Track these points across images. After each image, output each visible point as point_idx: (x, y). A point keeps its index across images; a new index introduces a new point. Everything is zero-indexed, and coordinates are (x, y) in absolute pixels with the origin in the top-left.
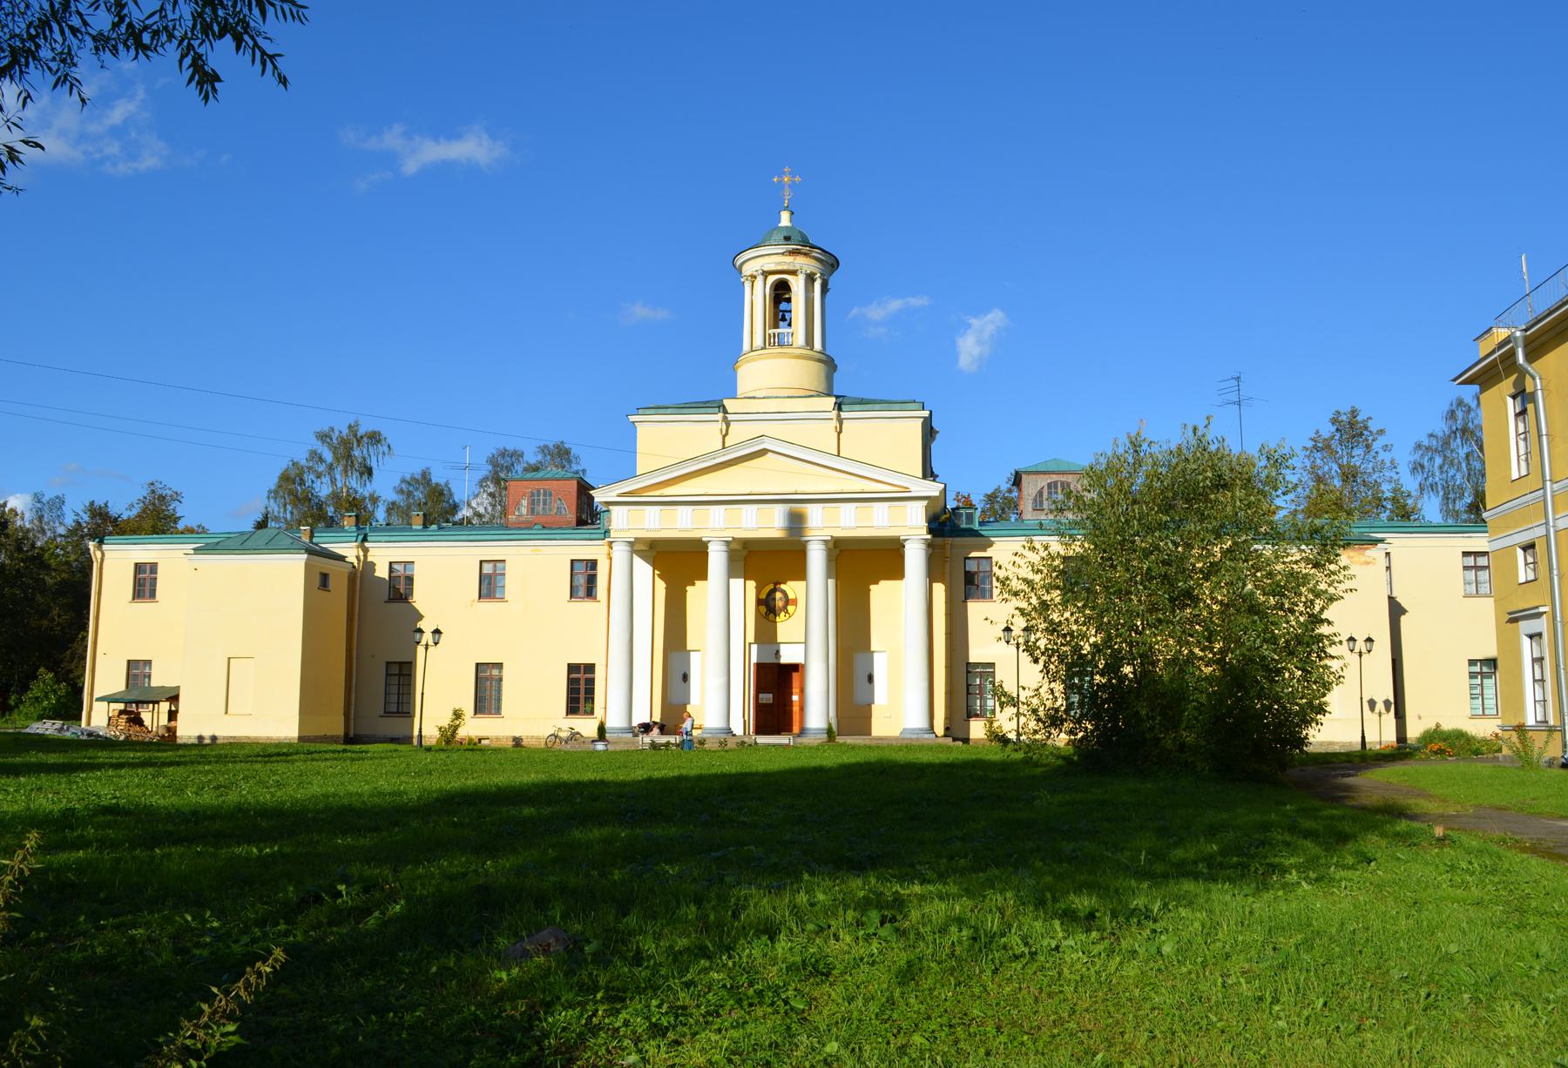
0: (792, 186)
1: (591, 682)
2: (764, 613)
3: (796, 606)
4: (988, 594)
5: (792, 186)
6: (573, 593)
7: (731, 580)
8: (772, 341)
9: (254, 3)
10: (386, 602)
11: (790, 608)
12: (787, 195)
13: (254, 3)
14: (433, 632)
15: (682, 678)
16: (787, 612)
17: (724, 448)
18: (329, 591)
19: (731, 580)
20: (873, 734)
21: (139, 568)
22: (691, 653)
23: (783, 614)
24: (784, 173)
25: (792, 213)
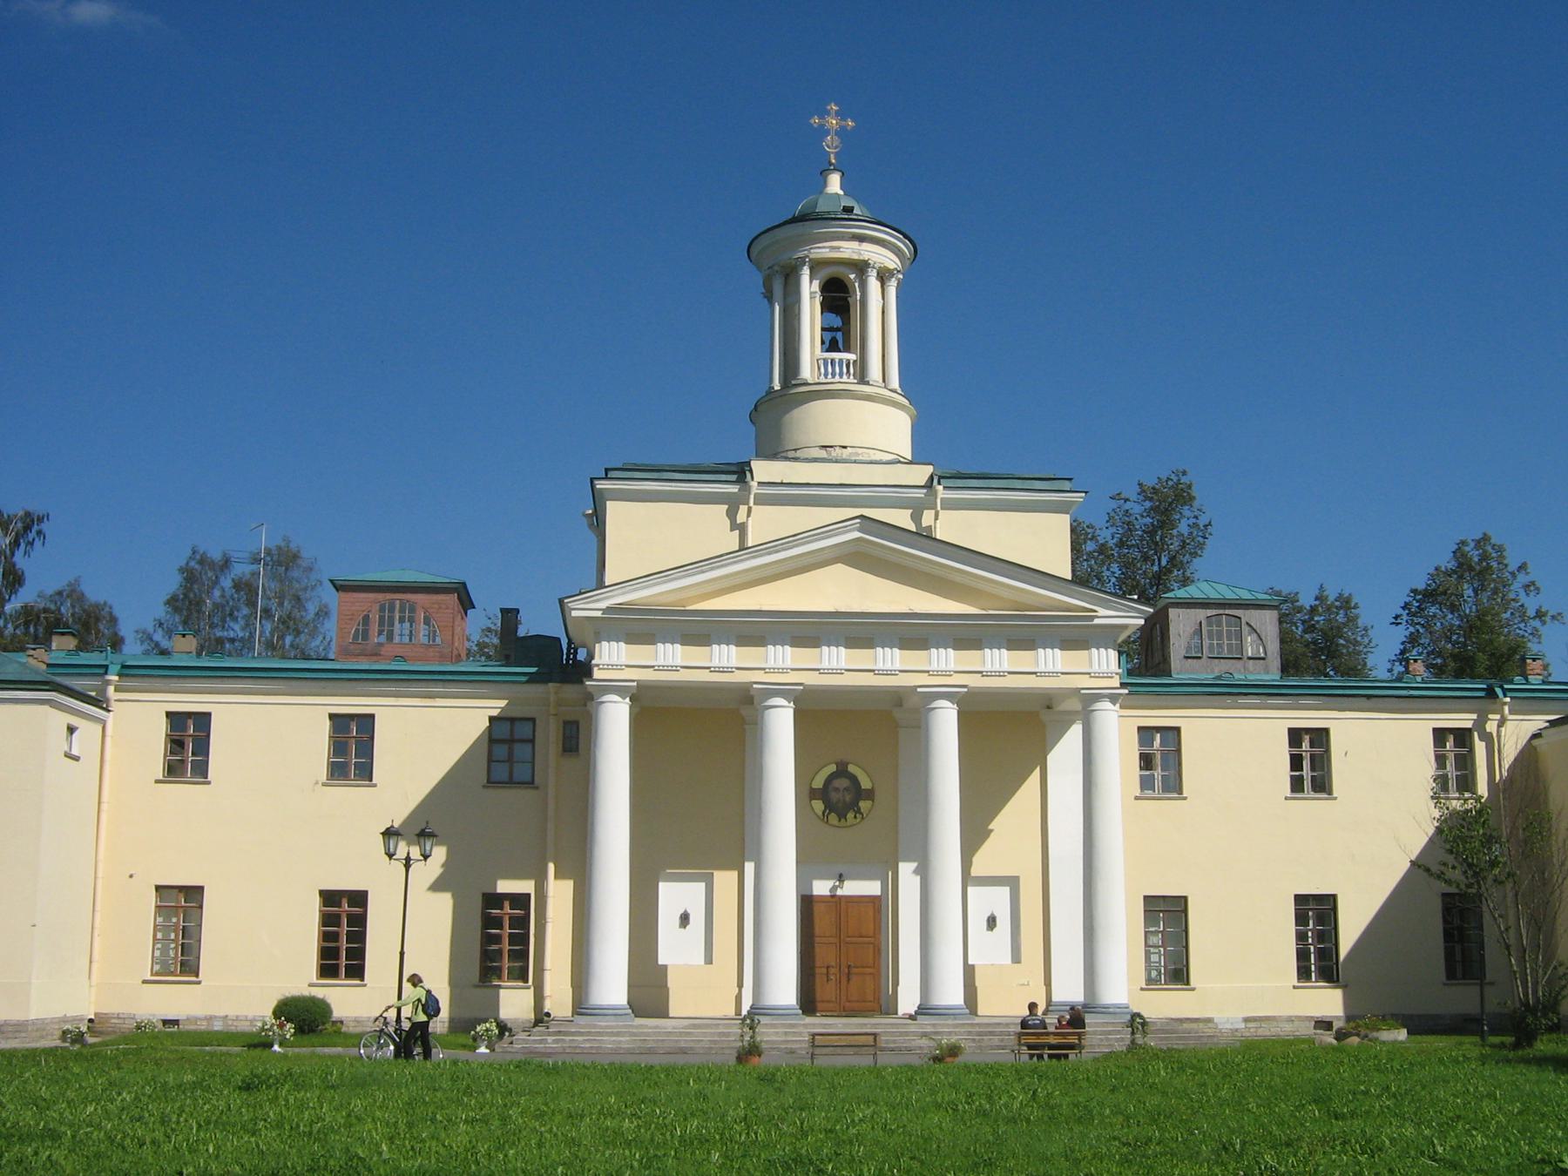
0: (841, 132)
1: (359, 921)
2: (820, 813)
3: (873, 801)
4: (501, 772)
5: (841, 132)
6: (1297, 785)
7: (671, 1015)
8: (822, 370)
9: (1096, 1175)
10: (157, 781)
11: (864, 805)
12: (831, 145)
13: (1096, 1175)
14: (382, 834)
15: (677, 921)
16: (859, 811)
17: (742, 547)
18: (1335, 798)
19: (671, 1015)
20: (879, 894)
21: (339, 722)
22: (700, 887)
23: (850, 815)
24: (828, 113)
25: (843, 174)
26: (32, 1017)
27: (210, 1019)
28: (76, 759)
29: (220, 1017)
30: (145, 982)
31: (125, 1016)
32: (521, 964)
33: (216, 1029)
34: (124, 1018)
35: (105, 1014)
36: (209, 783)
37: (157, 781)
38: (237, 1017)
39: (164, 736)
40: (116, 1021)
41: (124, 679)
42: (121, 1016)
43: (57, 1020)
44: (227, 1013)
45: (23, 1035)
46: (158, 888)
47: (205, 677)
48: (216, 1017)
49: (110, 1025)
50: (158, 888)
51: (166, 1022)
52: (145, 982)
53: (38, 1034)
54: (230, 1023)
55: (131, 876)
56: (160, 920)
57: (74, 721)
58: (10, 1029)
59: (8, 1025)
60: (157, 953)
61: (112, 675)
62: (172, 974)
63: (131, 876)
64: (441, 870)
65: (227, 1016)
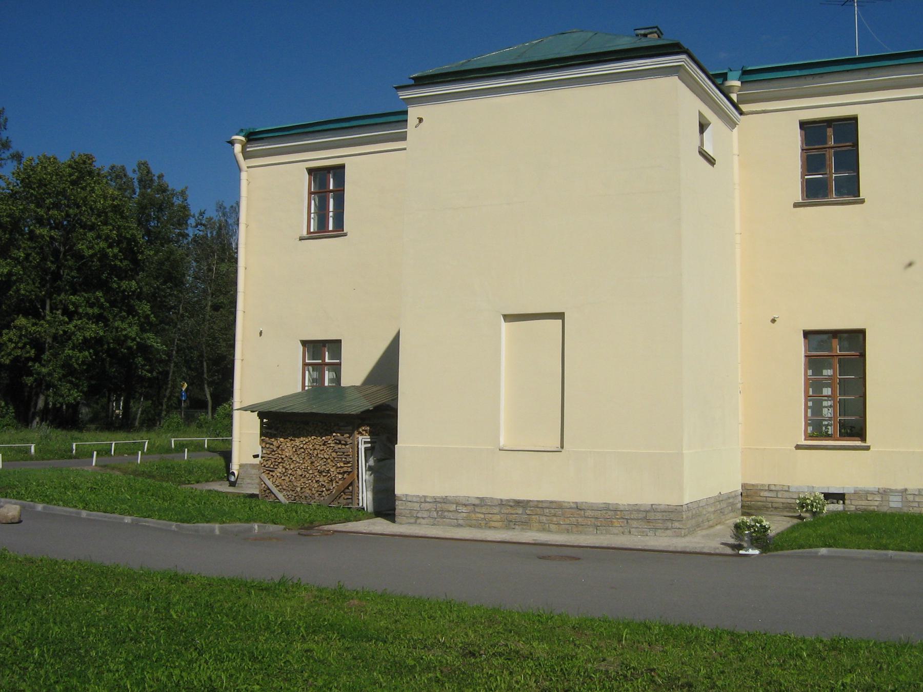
10: (796, 205)
26: (686, 500)
27: (885, 493)
28: (711, 161)
29: (896, 491)
30: (798, 447)
31: (778, 488)
32: (206, 386)
33: (892, 505)
34: (777, 491)
35: (753, 485)
36: (862, 201)
37: (796, 205)
38: (482, 499)
39: (800, 151)
40: (766, 494)
41: (748, 86)
42: (773, 488)
43: (712, 501)
44: (906, 487)
45: (677, 524)
46: (807, 334)
47: (848, 71)
48: (891, 491)
49: (759, 498)
50: (807, 334)
51: (828, 496)
52: (798, 447)
53: (693, 522)
54: (910, 498)
55: (773, 321)
56: (810, 372)
57: (709, 115)
58: (659, 516)
59: (655, 511)
60: (809, 414)
61: (733, 80)
62: (828, 436)
63: (773, 321)
64: (259, 420)
65: (906, 490)
